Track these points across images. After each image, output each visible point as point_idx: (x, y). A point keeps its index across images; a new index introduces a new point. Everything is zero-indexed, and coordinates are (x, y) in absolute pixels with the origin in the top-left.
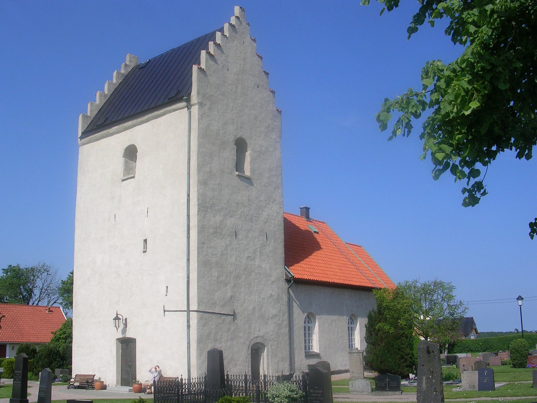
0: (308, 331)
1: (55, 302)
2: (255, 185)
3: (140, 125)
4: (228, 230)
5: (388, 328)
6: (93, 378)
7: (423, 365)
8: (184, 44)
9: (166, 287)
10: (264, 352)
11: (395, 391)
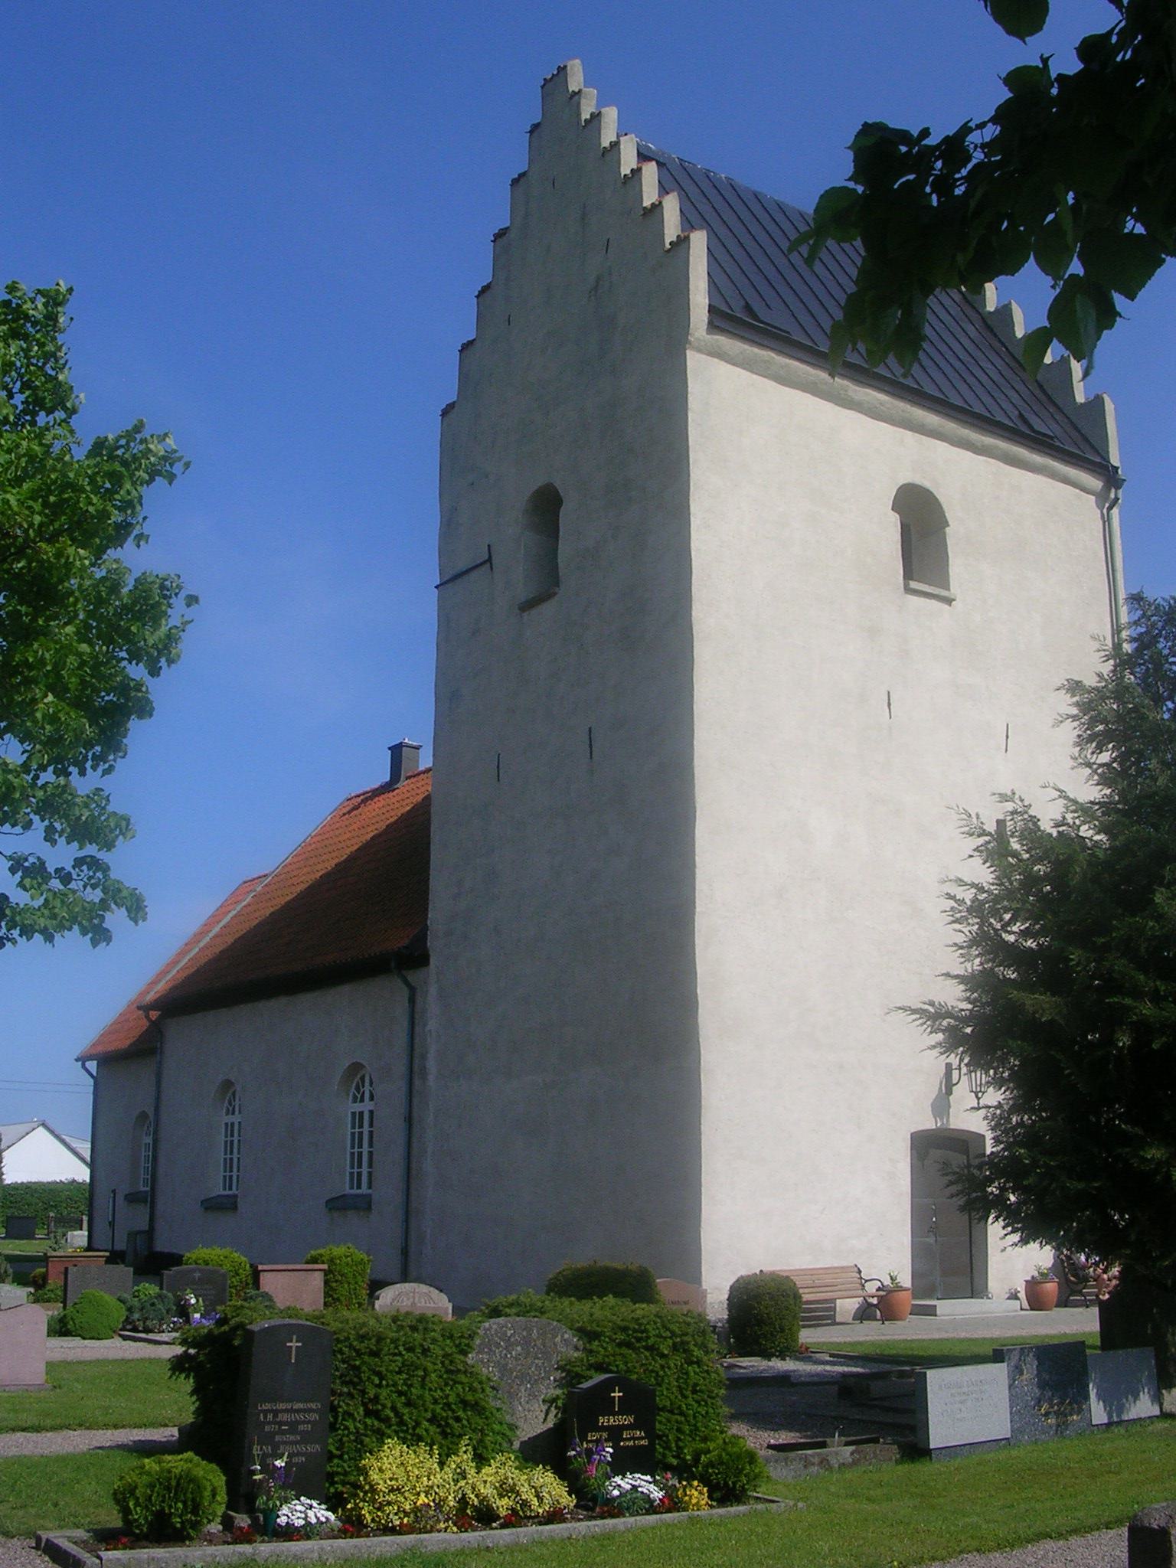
3: (952, 445)
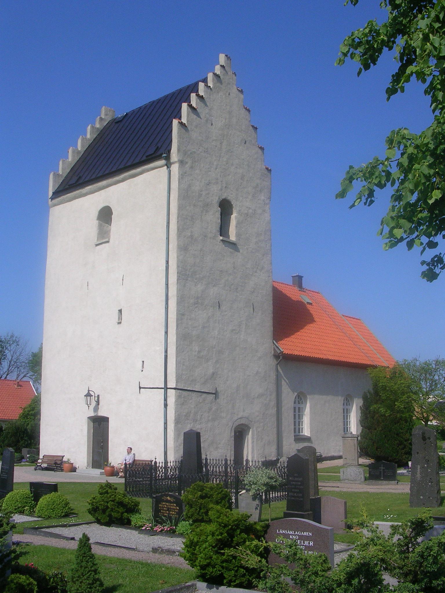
0: (298, 412)
1: (24, 376)
2: (241, 251)
4: (210, 300)
5: (384, 410)
6: (62, 459)
7: (418, 453)
8: (165, 96)
9: (142, 362)
10: (248, 435)
11: (390, 480)
